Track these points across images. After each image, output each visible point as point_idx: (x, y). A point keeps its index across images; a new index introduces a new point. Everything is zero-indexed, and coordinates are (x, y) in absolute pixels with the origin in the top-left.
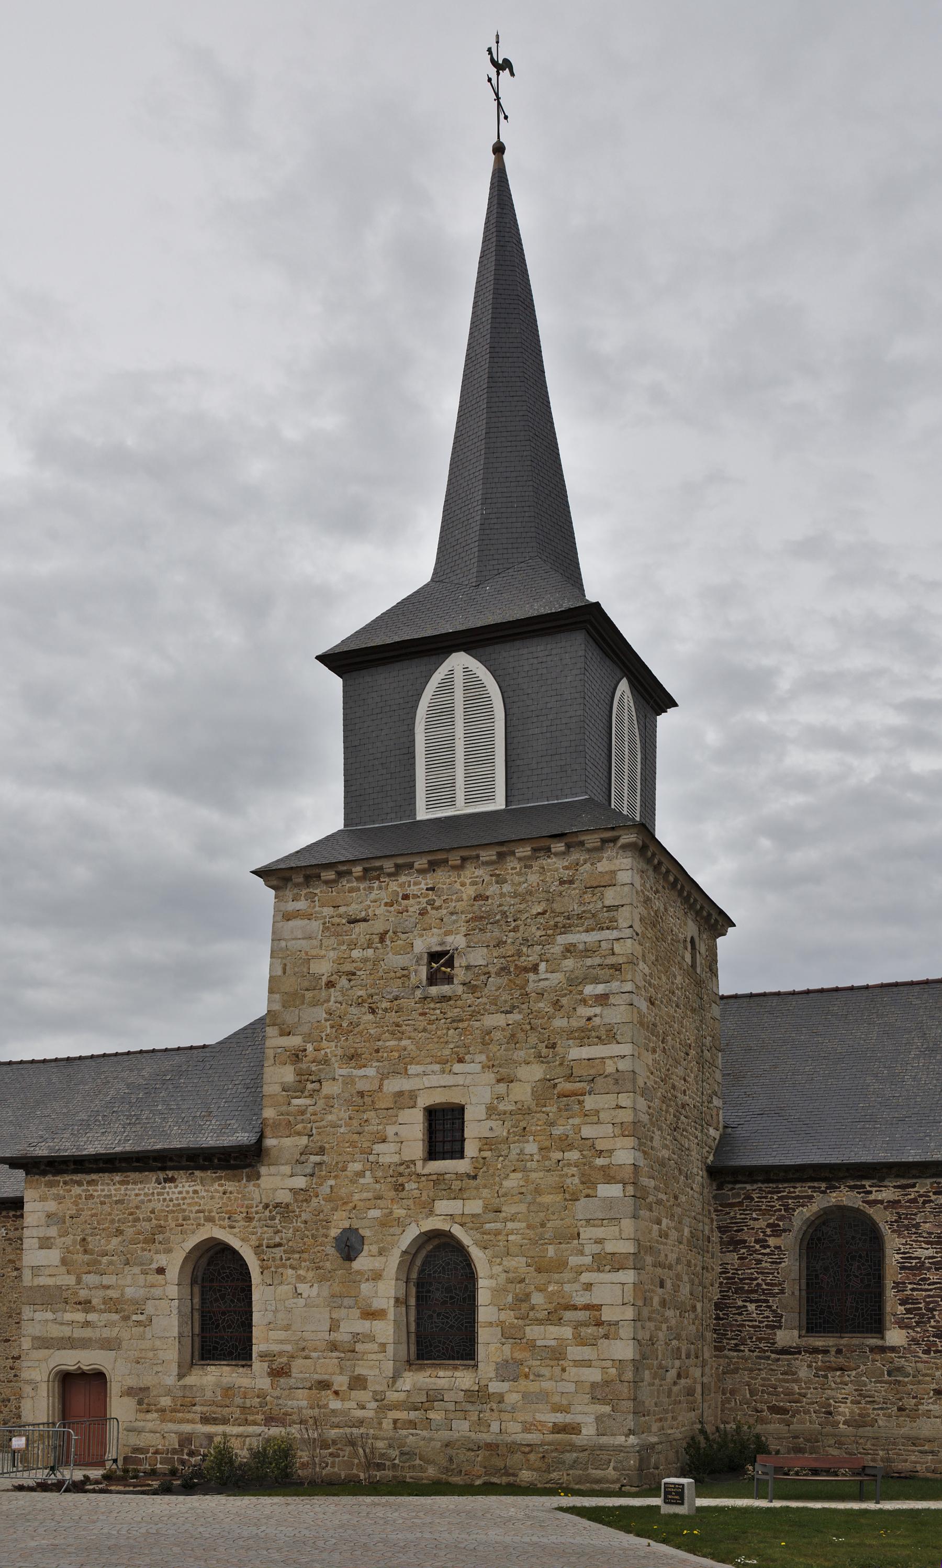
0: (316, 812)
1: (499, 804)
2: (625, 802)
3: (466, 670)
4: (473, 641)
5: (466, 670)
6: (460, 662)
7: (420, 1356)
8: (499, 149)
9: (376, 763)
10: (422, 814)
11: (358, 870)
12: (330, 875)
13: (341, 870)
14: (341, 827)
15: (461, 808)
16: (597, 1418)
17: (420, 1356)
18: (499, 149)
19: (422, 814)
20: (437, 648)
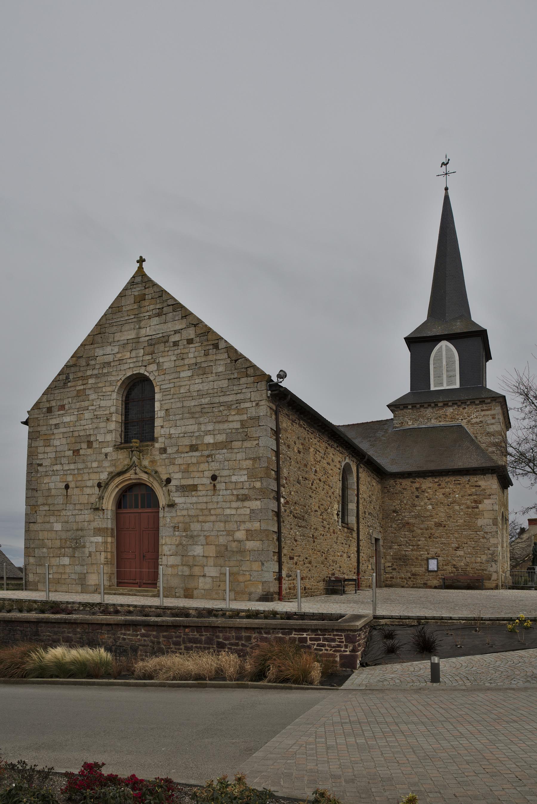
0: (402, 387)
1: (457, 386)
2: (484, 386)
3: (446, 346)
4: (449, 338)
5: (446, 346)
6: (444, 344)
7: (119, 584)
8: (446, 189)
9: (419, 371)
10: (432, 388)
11: (410, 407)
12: (402, 407)
13: (405, 407)
14: (409, 391)
15: (445, 387)
16: (154, 584)
17: (119, 584)
18: (446, 189)
19: (432, 388)
20: (437, 339)
